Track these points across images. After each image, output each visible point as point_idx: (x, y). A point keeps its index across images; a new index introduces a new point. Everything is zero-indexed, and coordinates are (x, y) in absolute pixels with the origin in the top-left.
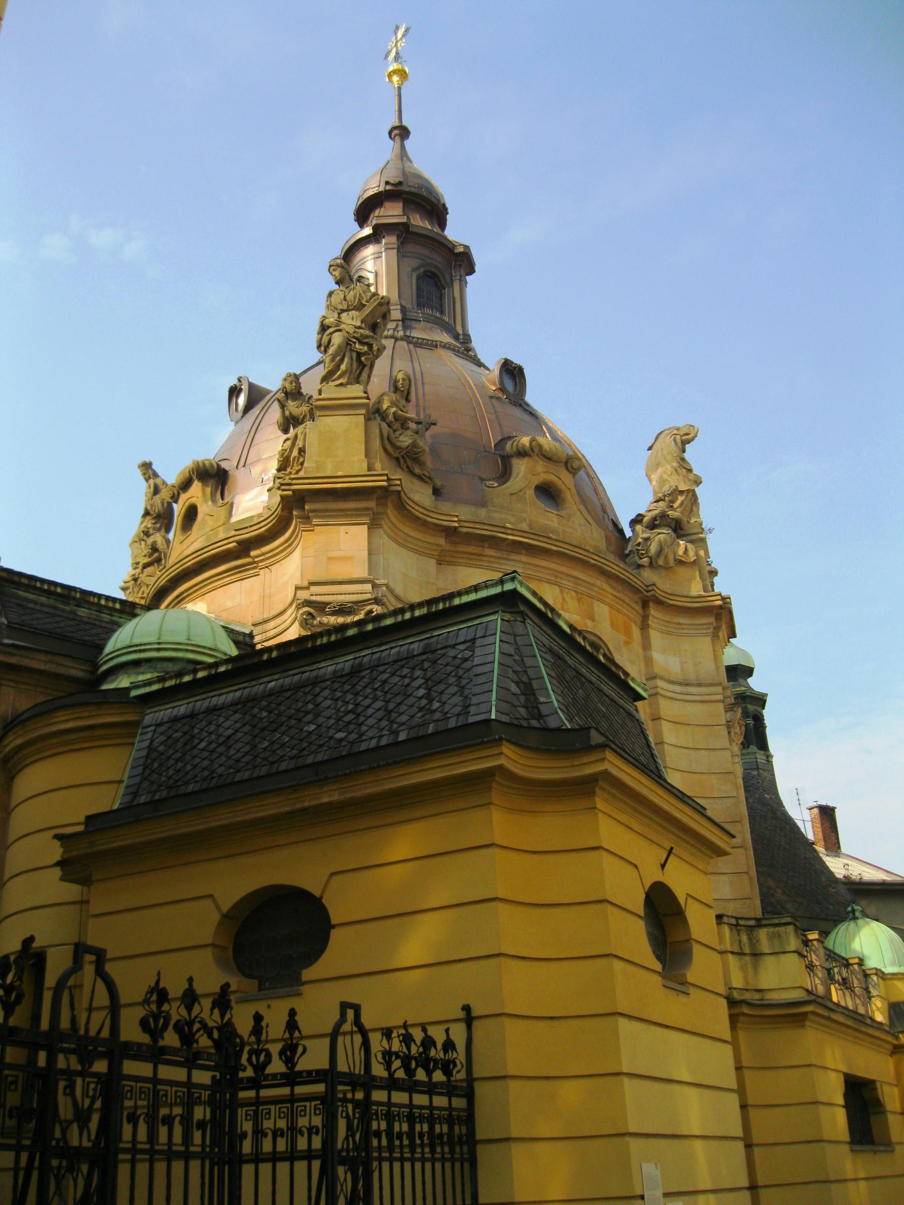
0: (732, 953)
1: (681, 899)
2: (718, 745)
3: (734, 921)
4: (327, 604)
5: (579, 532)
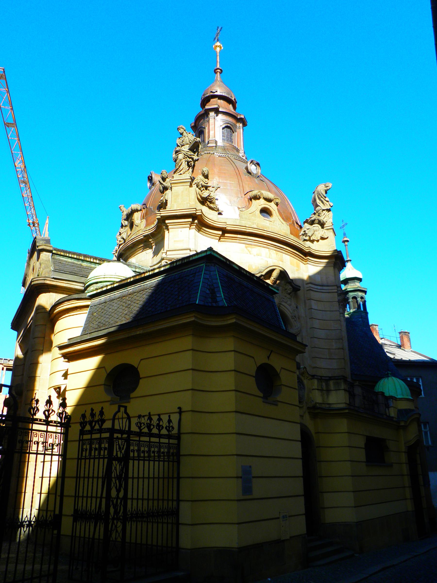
0: (318, 389)
1: (278, 371)
5: (278, 227)
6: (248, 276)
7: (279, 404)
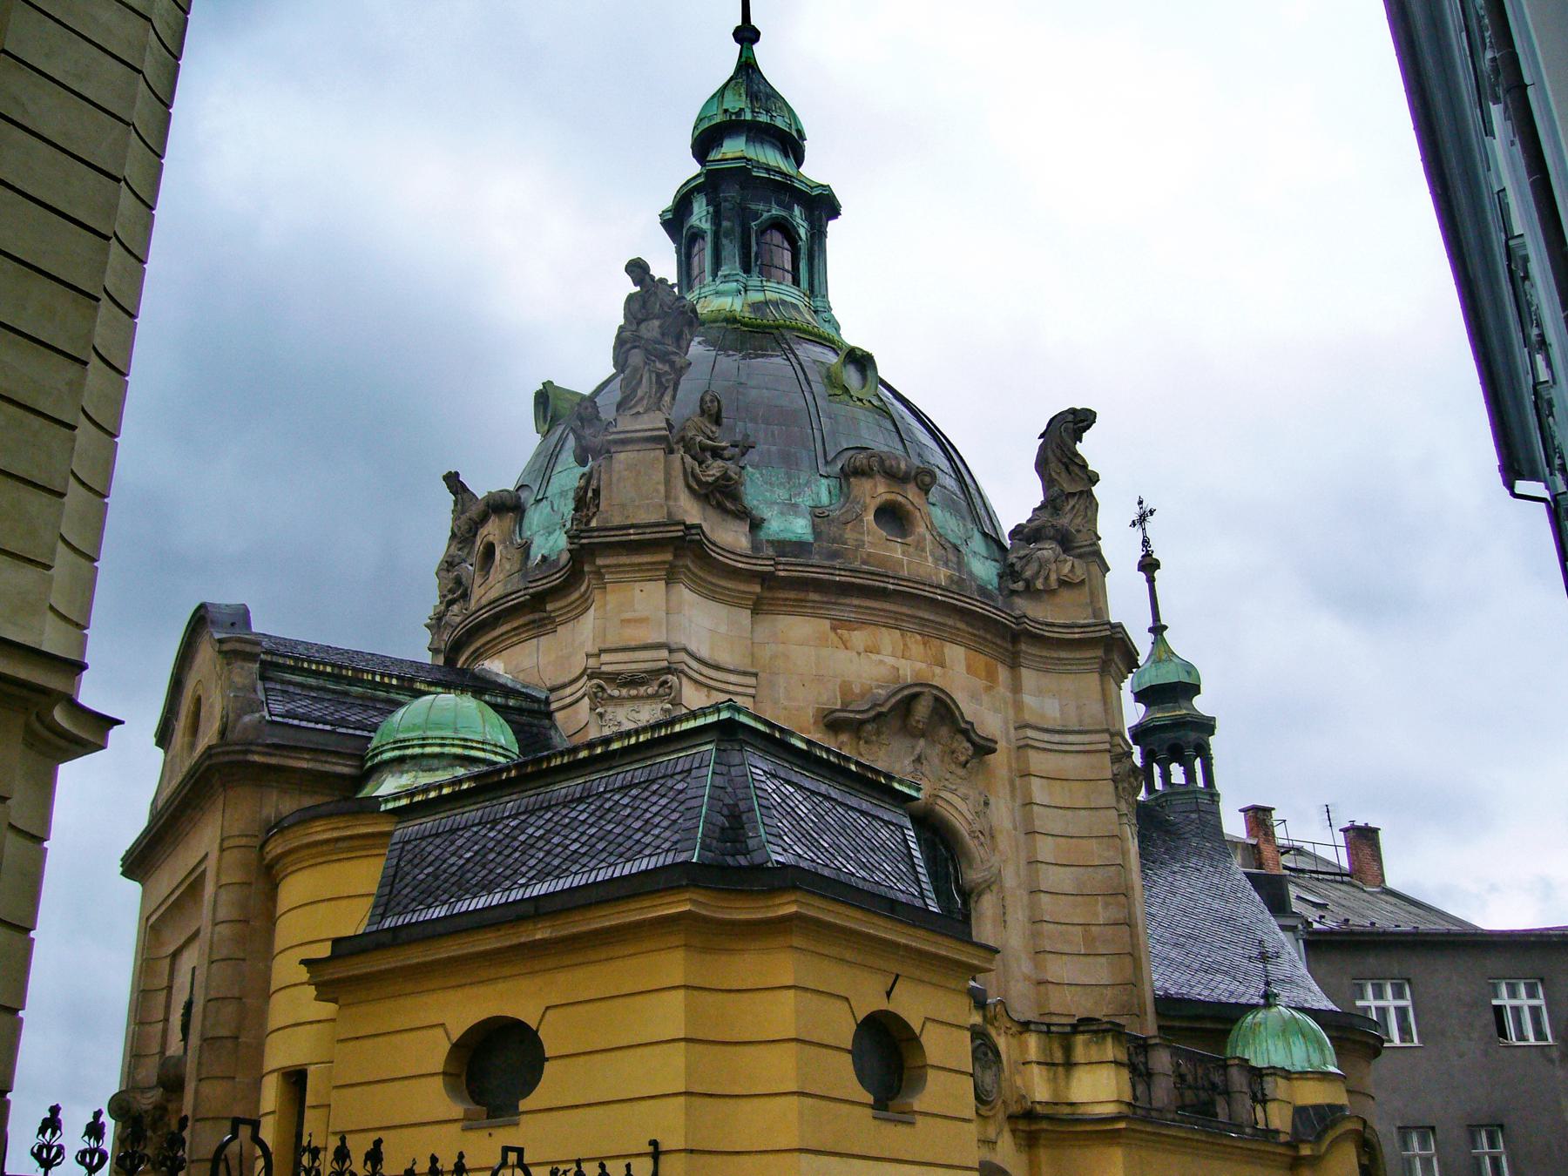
0: (1039, 1063)
2: (1101, 803)
3: (1044, 1028)
4: (619, 674)
6: (833, 763)
7: (919, 1120)
